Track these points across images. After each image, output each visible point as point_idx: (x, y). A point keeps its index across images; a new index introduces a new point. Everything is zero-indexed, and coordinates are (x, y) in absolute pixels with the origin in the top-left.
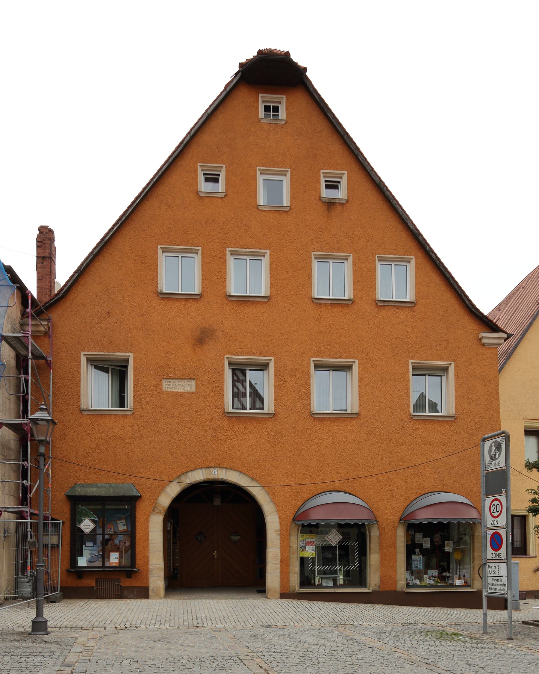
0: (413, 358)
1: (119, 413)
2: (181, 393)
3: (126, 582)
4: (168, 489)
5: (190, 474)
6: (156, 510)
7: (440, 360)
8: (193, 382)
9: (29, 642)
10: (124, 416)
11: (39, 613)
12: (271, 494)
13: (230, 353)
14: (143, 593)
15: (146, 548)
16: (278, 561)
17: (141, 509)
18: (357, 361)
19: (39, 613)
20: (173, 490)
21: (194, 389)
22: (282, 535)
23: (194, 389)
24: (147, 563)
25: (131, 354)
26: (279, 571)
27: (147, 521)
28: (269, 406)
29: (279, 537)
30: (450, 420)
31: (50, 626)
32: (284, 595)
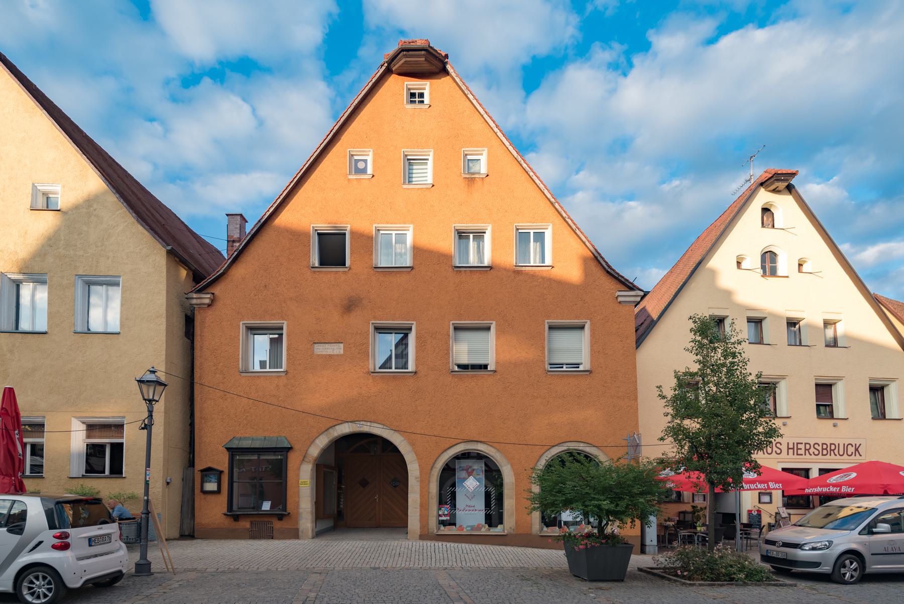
0: (549, 317)
1: (273, 374)
2: (330, 356)
3: (277, 525)
4: (317, 441)
5: (337, 427)
6: (306, 459)
7: (576, 318)
8: (342, 345)
9: (137, 579)
10: (278, 377)
11: (144, 556)
12: (412, 444)
13: (375, 318)
14: (295, 534)
15: (298, 493)
16: (418, 506)
17: (293, 459)
18: (494, 322)
19: (144, 556)
20: (322, 442)
21: (342, 352)
22: (421, 481)
23: (342, 352)
24: (298, 507)
25: (285, 322)
26: (418, 514)
27: (299, 469)
28: (411, 367)
29: (419, 484)
30: (254, 330)
31: (154, 567)
32: (424, 536)
